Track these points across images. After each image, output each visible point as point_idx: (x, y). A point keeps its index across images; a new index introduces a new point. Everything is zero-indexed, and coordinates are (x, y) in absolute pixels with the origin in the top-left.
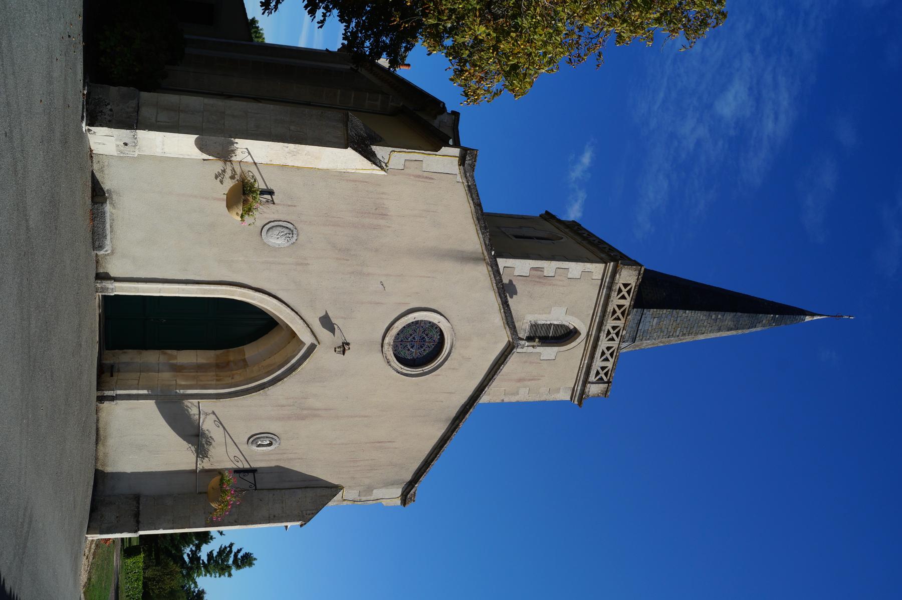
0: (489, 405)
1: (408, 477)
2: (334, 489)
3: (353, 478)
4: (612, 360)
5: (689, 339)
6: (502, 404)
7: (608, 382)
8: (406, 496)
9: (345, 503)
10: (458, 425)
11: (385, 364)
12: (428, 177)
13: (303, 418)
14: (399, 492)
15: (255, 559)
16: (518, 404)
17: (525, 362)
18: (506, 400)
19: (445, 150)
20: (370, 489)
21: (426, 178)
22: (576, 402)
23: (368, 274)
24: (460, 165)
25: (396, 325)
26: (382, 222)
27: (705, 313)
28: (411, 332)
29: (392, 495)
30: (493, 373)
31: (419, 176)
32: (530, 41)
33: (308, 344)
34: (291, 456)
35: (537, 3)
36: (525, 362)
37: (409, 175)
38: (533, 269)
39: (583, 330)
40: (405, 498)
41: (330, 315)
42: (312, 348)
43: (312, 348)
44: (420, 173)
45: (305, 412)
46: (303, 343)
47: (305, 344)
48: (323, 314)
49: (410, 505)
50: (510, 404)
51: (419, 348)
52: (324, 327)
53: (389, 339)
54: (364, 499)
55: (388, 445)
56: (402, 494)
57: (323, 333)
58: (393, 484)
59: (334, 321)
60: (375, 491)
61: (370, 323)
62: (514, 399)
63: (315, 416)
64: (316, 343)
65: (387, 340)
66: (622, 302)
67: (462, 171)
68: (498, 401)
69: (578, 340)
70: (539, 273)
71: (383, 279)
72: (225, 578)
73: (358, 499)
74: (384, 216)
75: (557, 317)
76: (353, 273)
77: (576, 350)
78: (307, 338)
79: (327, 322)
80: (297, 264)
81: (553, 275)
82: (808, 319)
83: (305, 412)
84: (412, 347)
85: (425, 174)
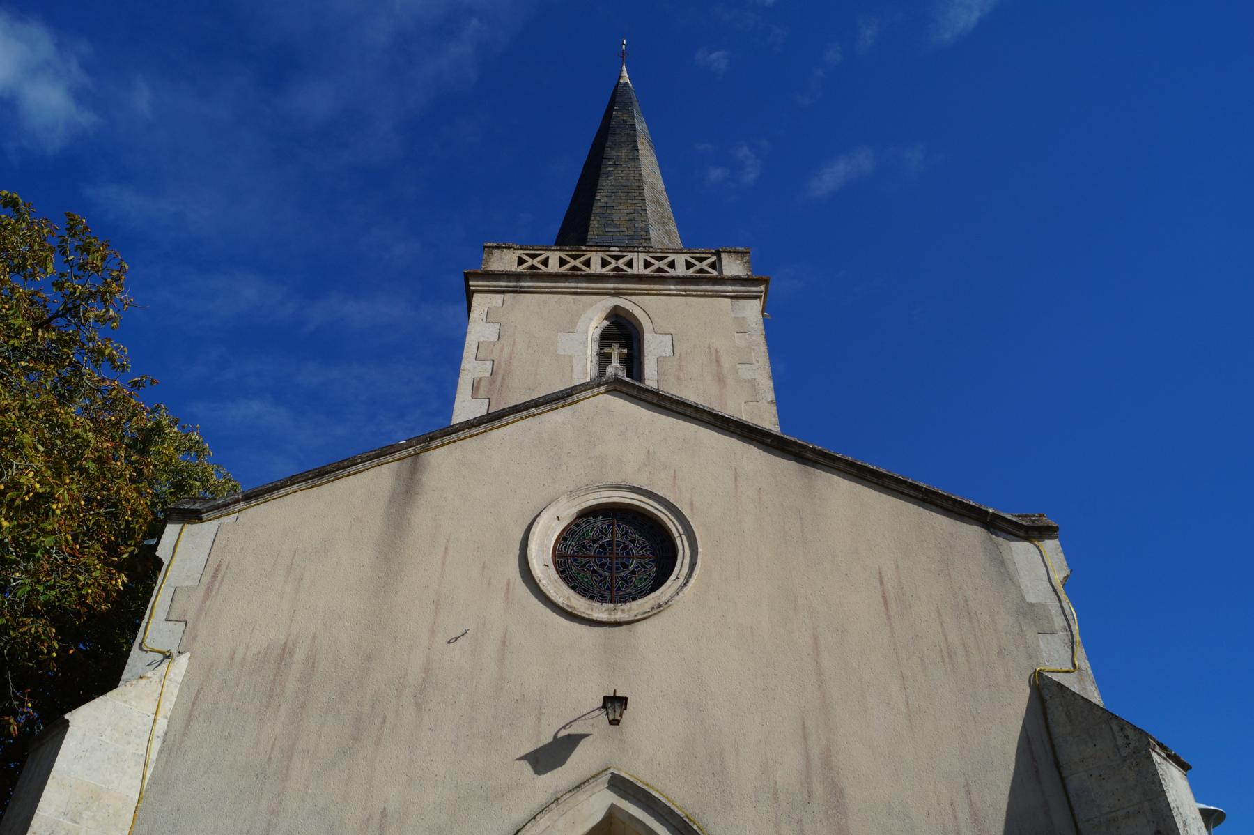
0: (781, 424)
1: (972, 533)
2: (1044, 693)
3: (1001, 651)
7: (718, 254)
8: (1027, 529)
10: (814, 451)
11: (665, 615)
12: (214, 575)
13: (837, 795)
14: (1021, 551)
15: (771, 402)
17: (679, 378)
18: (770, 396)
19: (163, 552)
20: (1027, 611)
21: (214, 577)
22: (762, 288)
23: (427, 671)
24: (201, 520)
25: (560, 601)
26: (300, 655)
27: (602, 178)
30: (681, 409)
31: (208, 590)
33: (611, 798)
36: (679, 378)
37: (201, 609)
38: (474, 395)
39: (607, 303)
40: (1034, 532)
41: (528, 749)
42: (619, 785)
43: (619, 785)
44: (201, 590)
45: (818, 788)
46: (612, 810)
47: (613, 807)
48: (526, 767)
50: (777, 389)
51: (622, 552)
52: (564, 763)
54: (1059, 622)
56: (1025, 539)
57: (580, 762)
58: (1004, 571)
59: (547, 739)
60: (1031, 598)
61: (563, 659)
63: (828, 762)
64: (607, 777)
65: (603, 616)
67: (214, 514)
68: (774, 409)
69: (638, 313)
70: (483, 384)
71: (441, 639)
72: (604, 314)
73: (1062, 634)
74: (285, 652)
76: (418, 706)
77: (647, 308)
78: (598, 803)
79: (548, 757)
81: (489, 365)
82: (625, 78)
83: (818, 788)
84: (626, 567)
85: (207, 579)
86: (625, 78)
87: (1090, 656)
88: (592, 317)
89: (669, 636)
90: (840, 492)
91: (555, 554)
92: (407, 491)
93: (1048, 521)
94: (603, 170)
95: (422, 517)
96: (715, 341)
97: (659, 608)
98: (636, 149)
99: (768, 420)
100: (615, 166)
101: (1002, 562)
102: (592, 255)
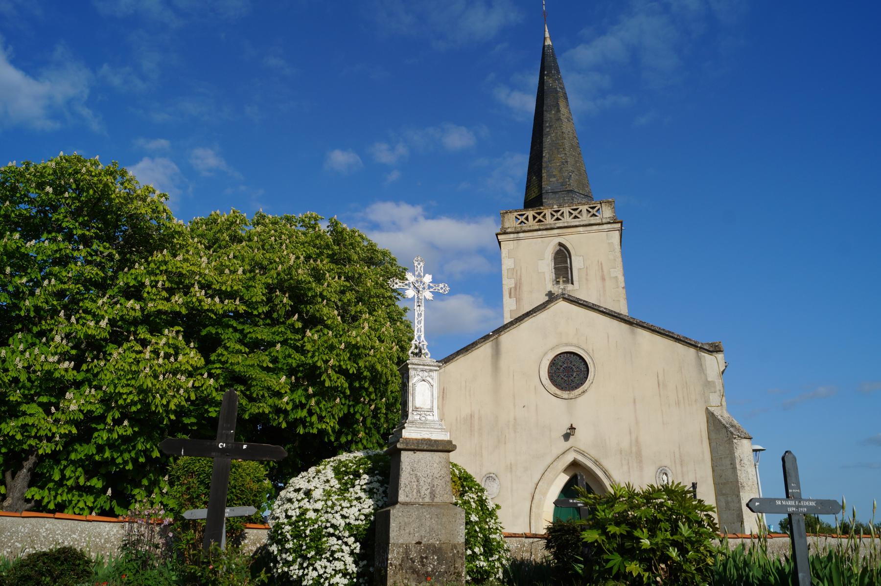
1: (692, 351)
3: (696, 401)
4: (581, 208)
5: (224, 531)
6: (628, 287)
9: (724, 403)
11: (586, 394)
16: (626, 274)
17: (587, 280)
18: (623, 285)
20: (708, 384)
23: (515, 419)
26: (476, 417)
28: (560, 379)
29: (714, 363)
32: (276, 231)
34: (677, 456)
35: (831, 580)
36: (587, 280)
38: (510, 297)
40: (714, 349)
49: (723, 346)
50: (626, 281)
51: (569, 372)
53: (565, 394)
55: (660, 378)
60: (709, 379)
61: (555, 408)
62: (621, 279)
66: (531, 218)
68: (624, 291)
70: (513, 291)
75: (547, 267)
76: (515, 432)
80: (511, 471)
82: (548, 42)
86: (548, 42)
87: (726, 401)
88: (548, 245)
89: (588, 406)
90: (644, 335)
91: (549, 373)
92: (497, 352)
93: (752, 436)
94: (545, 132)
95: (504, 362)
96: (598, 251)
97: (596, 462)
98: (558, 111)
99: (623, 309)
100: (550, 127)
101: (701, 365)
102: (546, 211)
